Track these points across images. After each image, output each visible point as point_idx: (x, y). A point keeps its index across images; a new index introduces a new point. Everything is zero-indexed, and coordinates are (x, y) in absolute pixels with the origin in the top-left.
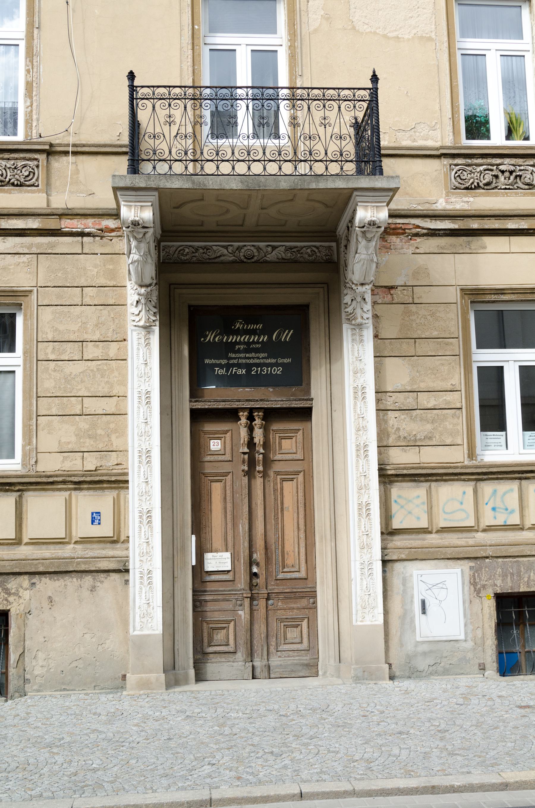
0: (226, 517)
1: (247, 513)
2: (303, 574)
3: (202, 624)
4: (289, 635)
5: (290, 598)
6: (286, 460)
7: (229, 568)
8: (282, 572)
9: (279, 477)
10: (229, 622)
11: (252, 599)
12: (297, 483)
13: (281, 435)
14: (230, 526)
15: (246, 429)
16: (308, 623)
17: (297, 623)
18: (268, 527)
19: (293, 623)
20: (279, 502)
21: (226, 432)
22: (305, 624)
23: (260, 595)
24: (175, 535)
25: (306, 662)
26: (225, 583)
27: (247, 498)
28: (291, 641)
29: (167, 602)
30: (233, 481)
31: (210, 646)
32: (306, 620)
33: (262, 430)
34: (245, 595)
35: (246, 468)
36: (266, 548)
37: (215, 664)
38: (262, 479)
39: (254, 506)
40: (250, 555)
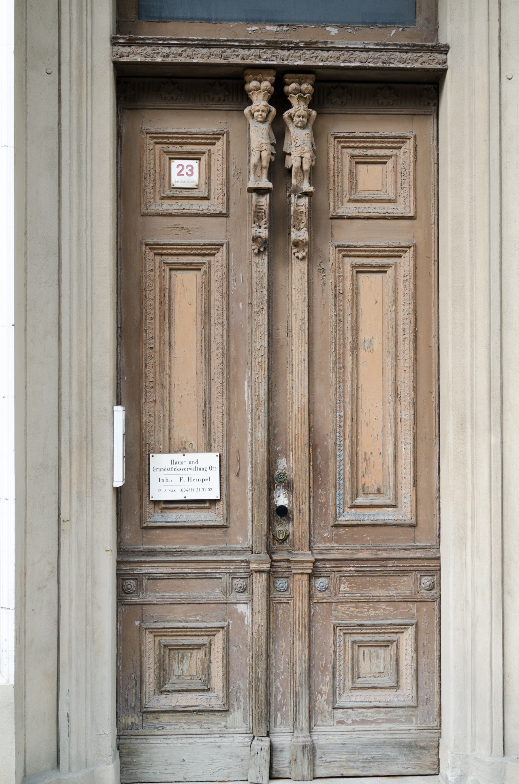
0: (208, 361)
1: (264, 352)
2: (404, 513)
3: (141, 636)
4: (365, 666)
5: (372, 574)
6: (368, 218)
7: (215, 495)
8: (352, 507)
9: (349, 261)
10: (211, 632)
11: (272, 574)
12: (396, 277)
13: (357, 152)
14: (217, 384)
15: (265, 127)
16: (416, 639)
17: (388, 637)
18: (319, 389)
19: (377, 637)
20: (348, 326)
21: (212, 139)
22: (407, 640)
23: (293, 566)
24: (65, 404)
25: (407, 738)
26: (203, 532)
27: (265, 312)
28: (372, 682)
29: (39, 588)
30: (228, 268)
31: (162, 692)
32: (411, 631)
33: (307, 132)
34: (254, 566)
35: (264, 233)
36: (313, 445)
37: (172, 741)
38: (304, 265)
39: (281, 334)
40: (269, 460)
